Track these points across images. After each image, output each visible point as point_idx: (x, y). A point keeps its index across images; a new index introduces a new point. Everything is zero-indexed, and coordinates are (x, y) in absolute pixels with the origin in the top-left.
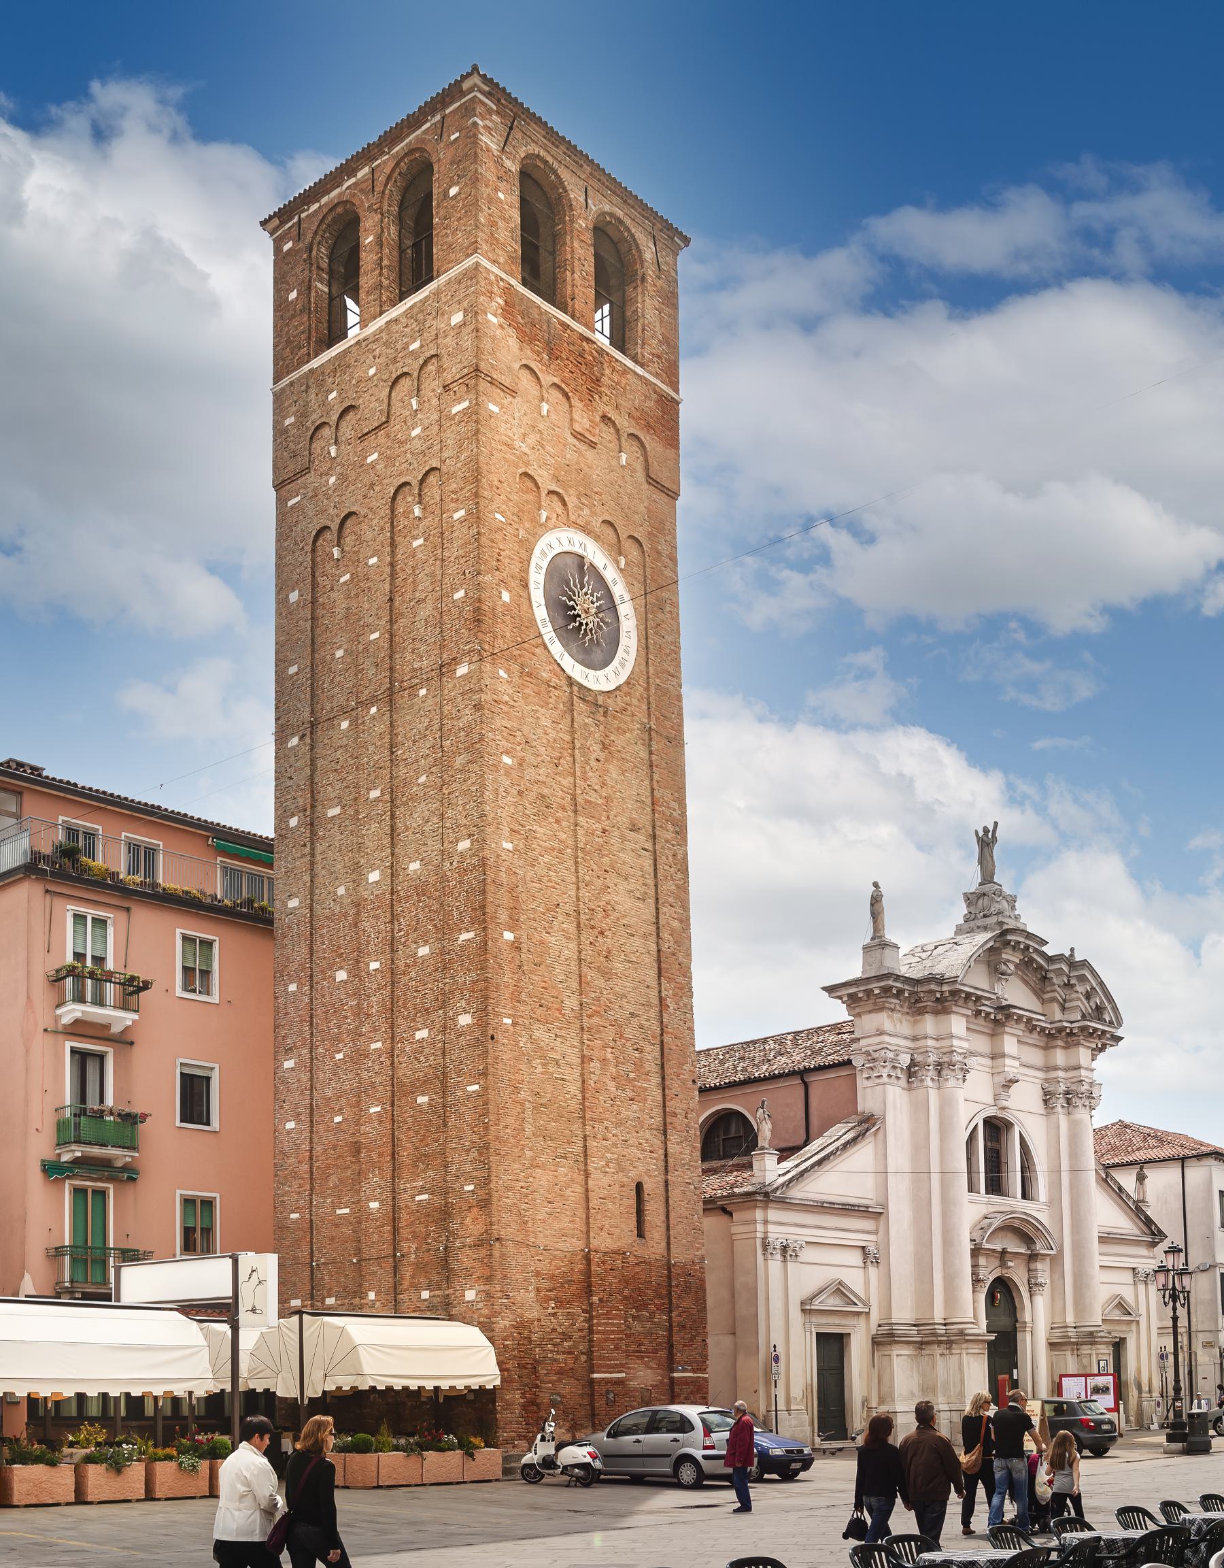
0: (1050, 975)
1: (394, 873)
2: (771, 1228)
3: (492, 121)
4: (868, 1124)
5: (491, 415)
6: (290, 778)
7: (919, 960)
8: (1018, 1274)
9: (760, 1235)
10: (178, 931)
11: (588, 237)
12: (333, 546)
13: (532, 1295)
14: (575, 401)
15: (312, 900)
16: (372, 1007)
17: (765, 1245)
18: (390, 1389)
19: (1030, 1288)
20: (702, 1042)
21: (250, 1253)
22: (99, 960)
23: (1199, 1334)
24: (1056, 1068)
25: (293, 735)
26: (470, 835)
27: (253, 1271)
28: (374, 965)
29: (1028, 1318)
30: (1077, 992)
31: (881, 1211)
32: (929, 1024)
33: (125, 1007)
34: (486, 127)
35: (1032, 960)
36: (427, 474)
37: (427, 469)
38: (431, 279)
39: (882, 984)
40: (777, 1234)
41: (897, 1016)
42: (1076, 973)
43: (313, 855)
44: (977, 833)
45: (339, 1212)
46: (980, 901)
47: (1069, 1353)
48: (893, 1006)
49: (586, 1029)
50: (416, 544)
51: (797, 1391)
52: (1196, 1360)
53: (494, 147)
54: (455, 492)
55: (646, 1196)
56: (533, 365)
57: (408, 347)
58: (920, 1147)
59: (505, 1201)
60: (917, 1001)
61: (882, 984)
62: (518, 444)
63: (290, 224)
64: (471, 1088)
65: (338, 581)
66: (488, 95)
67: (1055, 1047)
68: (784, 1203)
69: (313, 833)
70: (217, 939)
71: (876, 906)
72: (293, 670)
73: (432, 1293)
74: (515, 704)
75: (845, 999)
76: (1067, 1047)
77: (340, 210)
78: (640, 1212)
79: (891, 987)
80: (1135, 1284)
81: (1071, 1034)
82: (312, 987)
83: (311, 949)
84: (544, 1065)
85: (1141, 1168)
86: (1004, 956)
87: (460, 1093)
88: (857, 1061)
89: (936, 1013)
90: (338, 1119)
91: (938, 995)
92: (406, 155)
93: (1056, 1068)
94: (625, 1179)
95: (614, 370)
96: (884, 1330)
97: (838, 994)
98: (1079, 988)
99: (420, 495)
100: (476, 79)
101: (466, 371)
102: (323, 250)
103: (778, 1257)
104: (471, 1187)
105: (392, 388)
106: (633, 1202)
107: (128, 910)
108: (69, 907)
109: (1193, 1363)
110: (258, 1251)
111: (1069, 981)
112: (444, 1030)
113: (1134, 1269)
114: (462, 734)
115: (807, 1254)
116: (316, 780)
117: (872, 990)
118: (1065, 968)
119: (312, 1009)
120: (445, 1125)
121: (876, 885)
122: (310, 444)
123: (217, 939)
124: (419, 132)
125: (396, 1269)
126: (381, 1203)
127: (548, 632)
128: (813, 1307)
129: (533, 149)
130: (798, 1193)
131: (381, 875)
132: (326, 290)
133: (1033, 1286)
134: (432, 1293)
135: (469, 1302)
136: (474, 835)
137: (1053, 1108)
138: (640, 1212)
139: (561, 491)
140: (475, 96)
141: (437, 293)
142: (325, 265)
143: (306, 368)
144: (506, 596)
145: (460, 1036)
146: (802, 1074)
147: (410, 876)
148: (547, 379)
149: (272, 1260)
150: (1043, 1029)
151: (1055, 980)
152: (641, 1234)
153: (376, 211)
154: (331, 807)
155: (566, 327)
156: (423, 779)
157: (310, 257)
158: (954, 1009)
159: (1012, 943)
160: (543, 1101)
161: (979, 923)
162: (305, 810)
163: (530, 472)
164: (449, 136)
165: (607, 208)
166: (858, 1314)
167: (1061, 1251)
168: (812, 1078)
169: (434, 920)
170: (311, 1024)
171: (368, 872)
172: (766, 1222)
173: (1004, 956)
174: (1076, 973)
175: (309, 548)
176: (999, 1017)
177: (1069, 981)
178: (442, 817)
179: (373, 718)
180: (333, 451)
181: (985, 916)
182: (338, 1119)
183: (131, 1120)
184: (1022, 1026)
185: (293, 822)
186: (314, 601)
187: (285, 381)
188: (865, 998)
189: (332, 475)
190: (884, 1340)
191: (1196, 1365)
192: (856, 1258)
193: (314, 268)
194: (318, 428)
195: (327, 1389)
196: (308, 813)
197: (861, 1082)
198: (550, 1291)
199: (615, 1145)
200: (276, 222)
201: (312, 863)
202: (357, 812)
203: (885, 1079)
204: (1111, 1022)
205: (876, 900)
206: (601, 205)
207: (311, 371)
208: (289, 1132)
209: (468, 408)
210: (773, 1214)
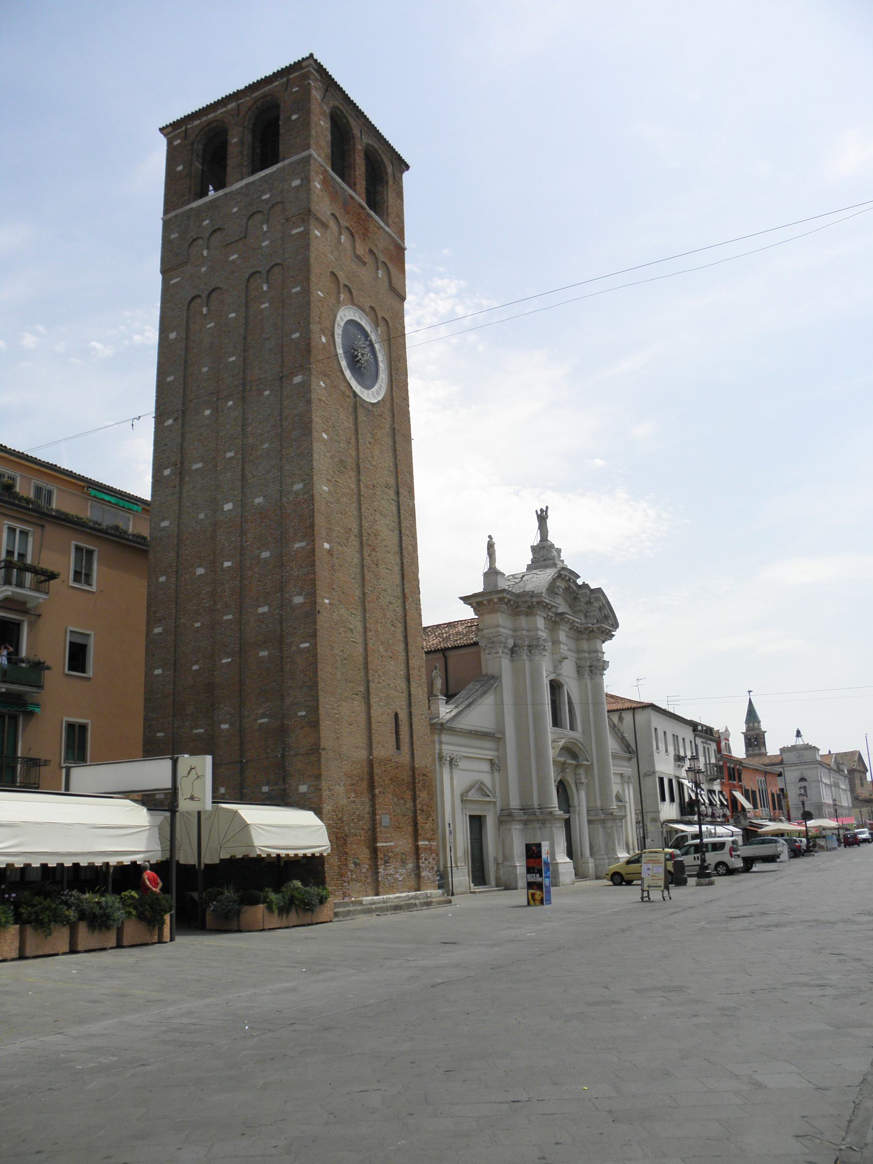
0: (579, 596)
1: (243, 505)
2: (444, 747)
3: (318, 84)
4: (490, 681)
5: (316, 237)
6: (166, 445)
7: (514, 583)
8: (570, 779)
9: (437, 751)
10: (73, 543)
11: (362, 155)
12: (203, 307)
13: (342, 788)
14: (357, 238)
15: (179, 521)
16: (225, 591)
17: (441, 758)
18: (76, 866)
19: (576, 785)
20: (428, 621)
21: (186, 756)
22: (22, 556)
23: (648, 814)
24: (584, 652)
25: (169, 418)
26: (303, 481)
27: (191, 769)
28: (227, 564)
29: (576, 805)
30: (594, 607)
31: (500, 736)
32: (523, 621)
33: (37, 590)
34: (315, 87)
35: (570, 587)
36: (272, 267)
37: (273, 263)
38: (277, 162)
39: (500, 596)
40: (447, 750)
41: (504, 615)
42: (594, 596)
43: (181, 493)
44: (536, 511)
45: (195, 731)
46: (541, 552)
47: (600, 826)
48: (503, 610)
49: (367, 610)
50: (263, 306)
51: (460, 853)
52: (647, 830)
53: (319, 98)
54: (293, 277)
55: (400, 722)
56: (337, 215)
57: (261, 198)
58: (519, 703)
59: (326, 724)
60: (516, 607)
61: (500, 596)
62: (329, 255)
63: (180, 130)
64: (303, 646)
65: (206, 327)
66: (317, 71)
67: (583, 639)
68: (453, 731)
69: (182, 479)
70: (96, 549)
71: (490, 550)
72: (170, 379)
73: (271, 788)
74: (329, 403)
75: (474, 605)
76: (588, 639)
77: (214, 124)
78: (397, 732)
79: (504, 598)
80: (622, 783)
81: (593, 631)
82: (177, 579)
83: (178, 553)
84: (345, 632)
85: (621, 714)
86: (557, 583)
87: (294, 648)
88: (482, 644)
89: (527, 614)
90: (195, 667)
91: (530, 604)
92: (261, 98)
93: (584, 652)
94: (389, 711)
95: (374, 226)
96: (505, 812)
97: (470, 602)
98: (596, 605)
99: (267, 278)
100: (311, 61)
101: (302, 211)
102: (200, 146)
103: (448, 765)
104: (303, 713)
105: (249, 219)
106: (394, 726)
107: (43, 526)
108: (5, 522)
109: (645, 832)
110: (193, 753)
111: (590, 600)
112: (281, 606)
113: (621, 774)
114: (297, 418)
115: (462, 764)
116: (185, 446)
117: (492, 600)
118: (588, 592)
119: (177, 594)
120: (282, 670)
121: (490, 537)
122: (189, 248)
123: (96, 549)
124: (271, 86)
125: (242, 772)
126: (231, 724)
127: (344, 363)
128: (468, 798)
129: (337, 104)
130: (460, 724)
131: (233, 506)
132: (200, 167)
133: (578, 784)
134: (271, 788)
135: (301, 794)
136: (306, 480)
137: (583, 675)
138: (397, 732)
139: (350, 286)
140: (310, 70)
141: (283, 169)
142: (200, 154)
143: (187, 207)
144: (324, 339)
145: (294, 610)
146: (444, 651)
147: (255, 507)
148: (344, 223)
149: (209, 759)
150: (577, 628)
151: (581, 599)
152: (398, 748)
153: (240, 126)
154: (196, 463)
155: (352, 198)
156: (266, 446)
157: (192, 148)
158: (539, 613)
159: (563, 576)
160: (346, 656)
161: (542, 564)
162: (176, 465)
163: (335, 272)
164: (292, 89)
165: (371, 142)
166: (490, 802)
167: (592, 763)
168: (449, 654)
169: (273, 535)
170: (176, 603)
171: (224, 504)
172: (441, 743)
173: (557, 583)
174: (594, 596)
175: (185, 308)
176: (558, 619)
177: (590, 600)
178: (281, 469)
179: (230, 407)
180: (205, 253)
181: (545, 560)
182: (195, 667)
183: (38, 666)
184: (568, 626)
185: (167, 472)
186: (187, 338)
187: (172, 214)
188: (487, 604)
189: (203, 267)
190: (505, 818)
191: (647, 833)
192: (486, 767)
193: (194, 155)
194: (195, 240)
195: (222, 857)
196: (179, 466)
197: (484, 656)
198: (351, 786)
199: (384, 688)
200: (170, 129)
201: (180, 498)
202: (216, 466)
203: (500, 654)
204: (612, 625)
205: (491, 547)
206: (366, 140)
207: (192, 209)
208: (157, 676)
209: (303, 231)
210: (445, 738)
